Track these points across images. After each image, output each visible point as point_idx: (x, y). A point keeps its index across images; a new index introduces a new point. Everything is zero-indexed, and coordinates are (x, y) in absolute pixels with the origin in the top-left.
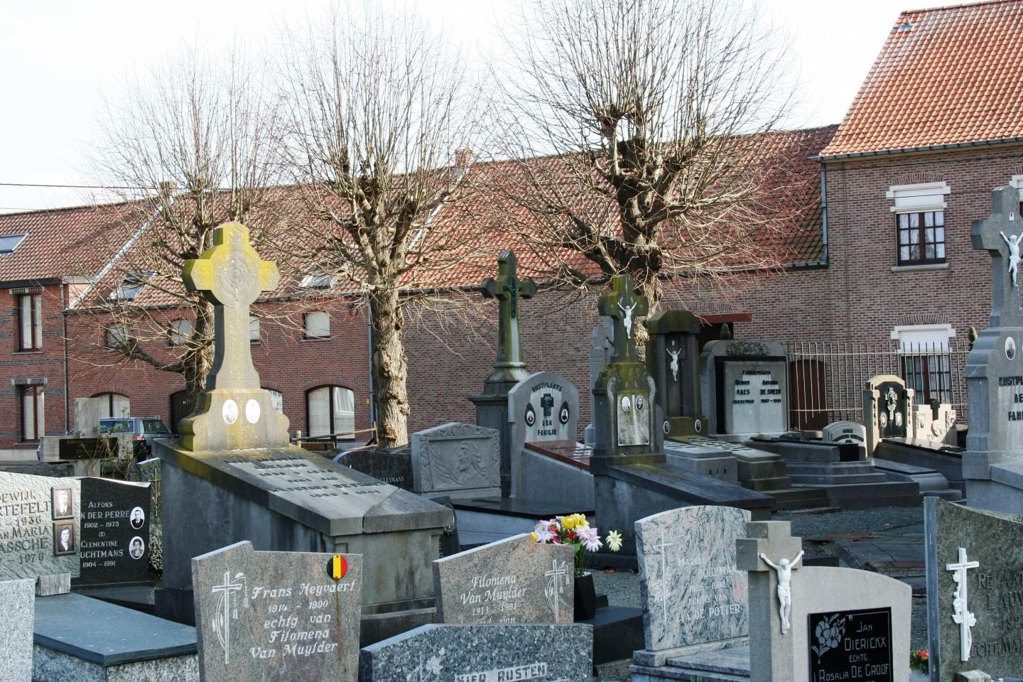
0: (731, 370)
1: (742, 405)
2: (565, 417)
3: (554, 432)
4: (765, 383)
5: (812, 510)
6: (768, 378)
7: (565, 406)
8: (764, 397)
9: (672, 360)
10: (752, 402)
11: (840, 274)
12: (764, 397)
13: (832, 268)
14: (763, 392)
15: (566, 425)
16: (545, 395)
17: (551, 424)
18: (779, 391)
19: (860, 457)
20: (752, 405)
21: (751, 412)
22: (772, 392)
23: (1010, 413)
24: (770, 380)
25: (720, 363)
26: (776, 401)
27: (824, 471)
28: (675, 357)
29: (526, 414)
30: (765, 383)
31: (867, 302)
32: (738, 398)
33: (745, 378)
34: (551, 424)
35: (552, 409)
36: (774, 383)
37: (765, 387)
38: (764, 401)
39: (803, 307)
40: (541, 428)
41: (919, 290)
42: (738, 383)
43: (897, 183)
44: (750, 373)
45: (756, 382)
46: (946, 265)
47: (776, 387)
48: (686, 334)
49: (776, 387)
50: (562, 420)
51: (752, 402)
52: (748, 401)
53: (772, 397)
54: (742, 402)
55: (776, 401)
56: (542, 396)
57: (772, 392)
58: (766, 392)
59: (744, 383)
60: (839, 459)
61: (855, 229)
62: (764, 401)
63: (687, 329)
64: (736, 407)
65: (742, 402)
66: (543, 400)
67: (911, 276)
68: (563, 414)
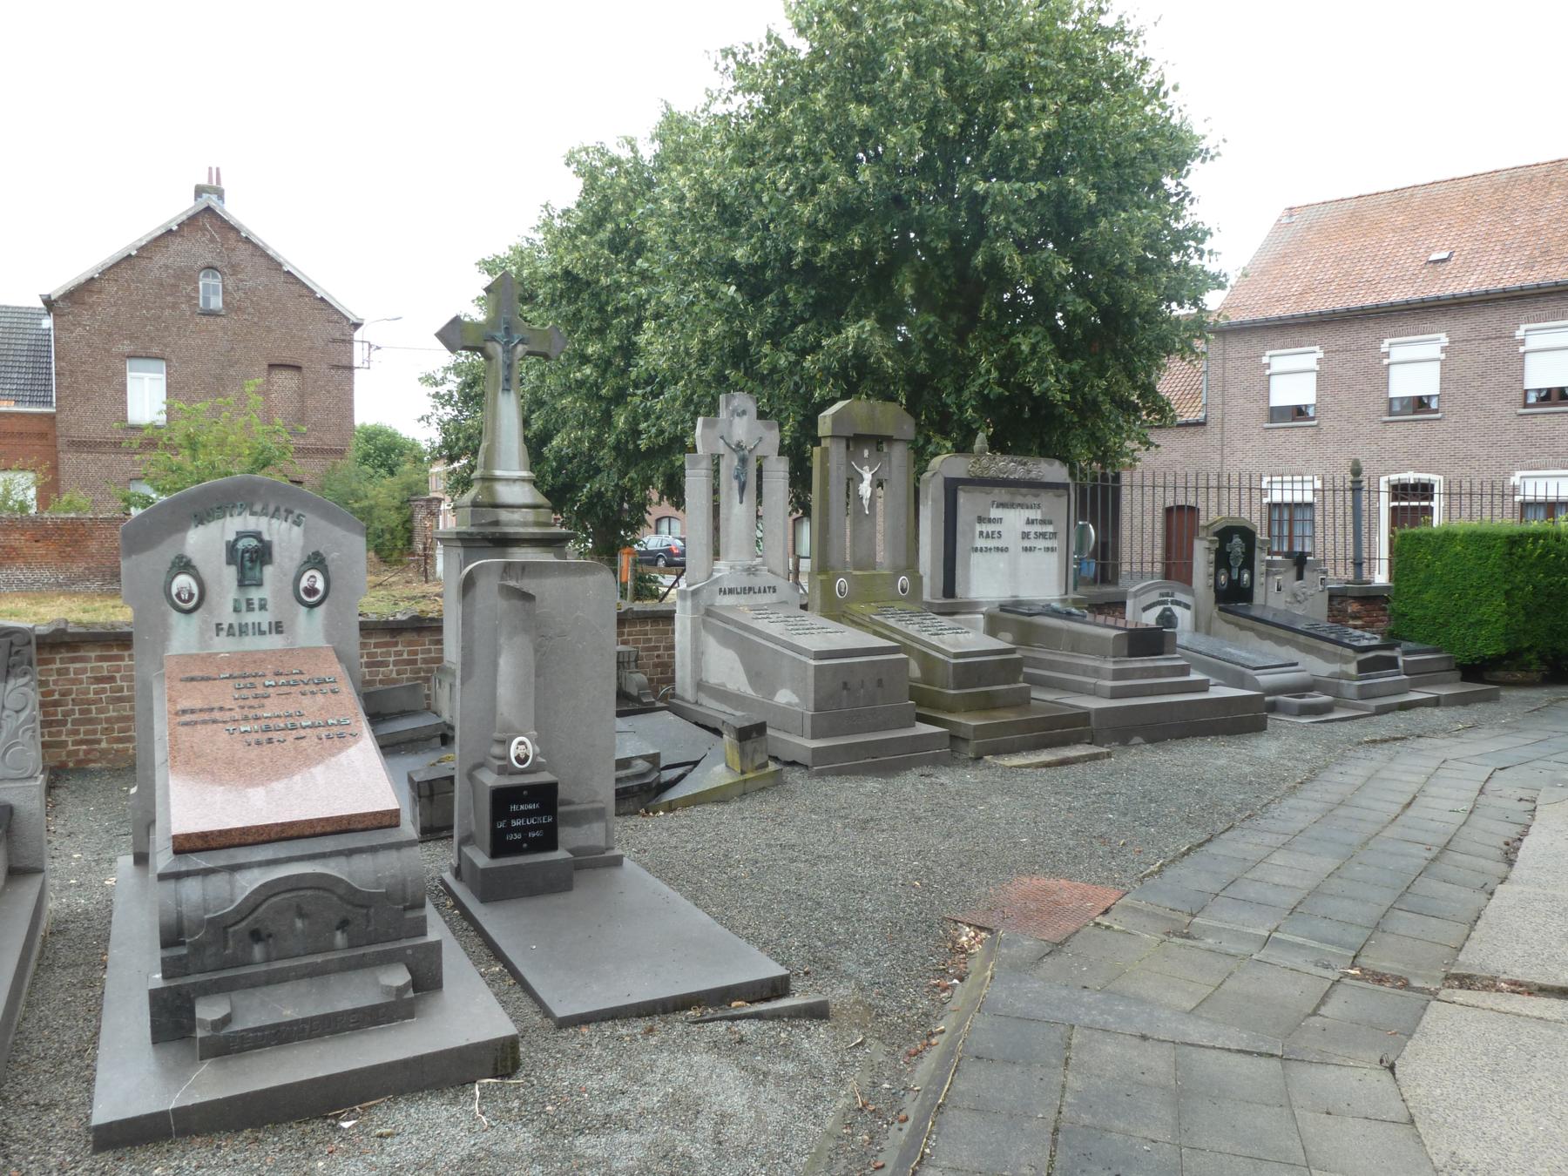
0: (967, 502)
1: (988, 555)
2: (311, 591)
3: (278, 628)
4: (1030, 522)
5: (1045, 756)
6: (1035, 514)
7: (316, 561)
8: (1027, 543)
9: (862, 480)
10: (1006, 550)
11: (1217, 430)
12: (1027, 543)
13: (1210, 424)
14: (1025, 535)
15: (320, 612)
16: (241, 535)
17: (263, 607)
18: (1054, 535)
19: (1166, 649)
20: (1005, 555)
21: (1002, 565)
22: (1043, 535)
23: (218, 625)
24: (1039, 517)
25: (952, 488)
26: (1047, 549)
27: (1096, 672)
28: (868, 476)
29: (298, 580)
30: (1030, 522)
31: (1239, 455)
32: (980, 543)
33: (995, 513)
34: (263, 607)
35: (268, 571)
36: (1043, 522)
37: (1027, 529)
38: (1026, 549)
39: (1182, 459)
40: (228, 617)
41: (1288, 445)
42: (981, 520)
43: (1273, 348)
44: (1002, 505)
45: (1014, 521)
46: (1315, 423)
47: (1050, 529)
48: (889, 440)
49: (1050, 529)
50: (309, 600)
51: (1006, 550)
52: (998, 549)
53: (1041, 544)
54: (988, 550)
55: (1047, 549)
56: (231, 537)
57: (1043, 535)
58: (1032, 535)
59: (990, 521)
60: (1126, 652)
61: (1232, 390)
62: (1026, 549)
63: (889, 433)
64: (976, 558)
65: (988, 550)
66: (231, 548)
67: (1282, 432)
68: (304, 583)
